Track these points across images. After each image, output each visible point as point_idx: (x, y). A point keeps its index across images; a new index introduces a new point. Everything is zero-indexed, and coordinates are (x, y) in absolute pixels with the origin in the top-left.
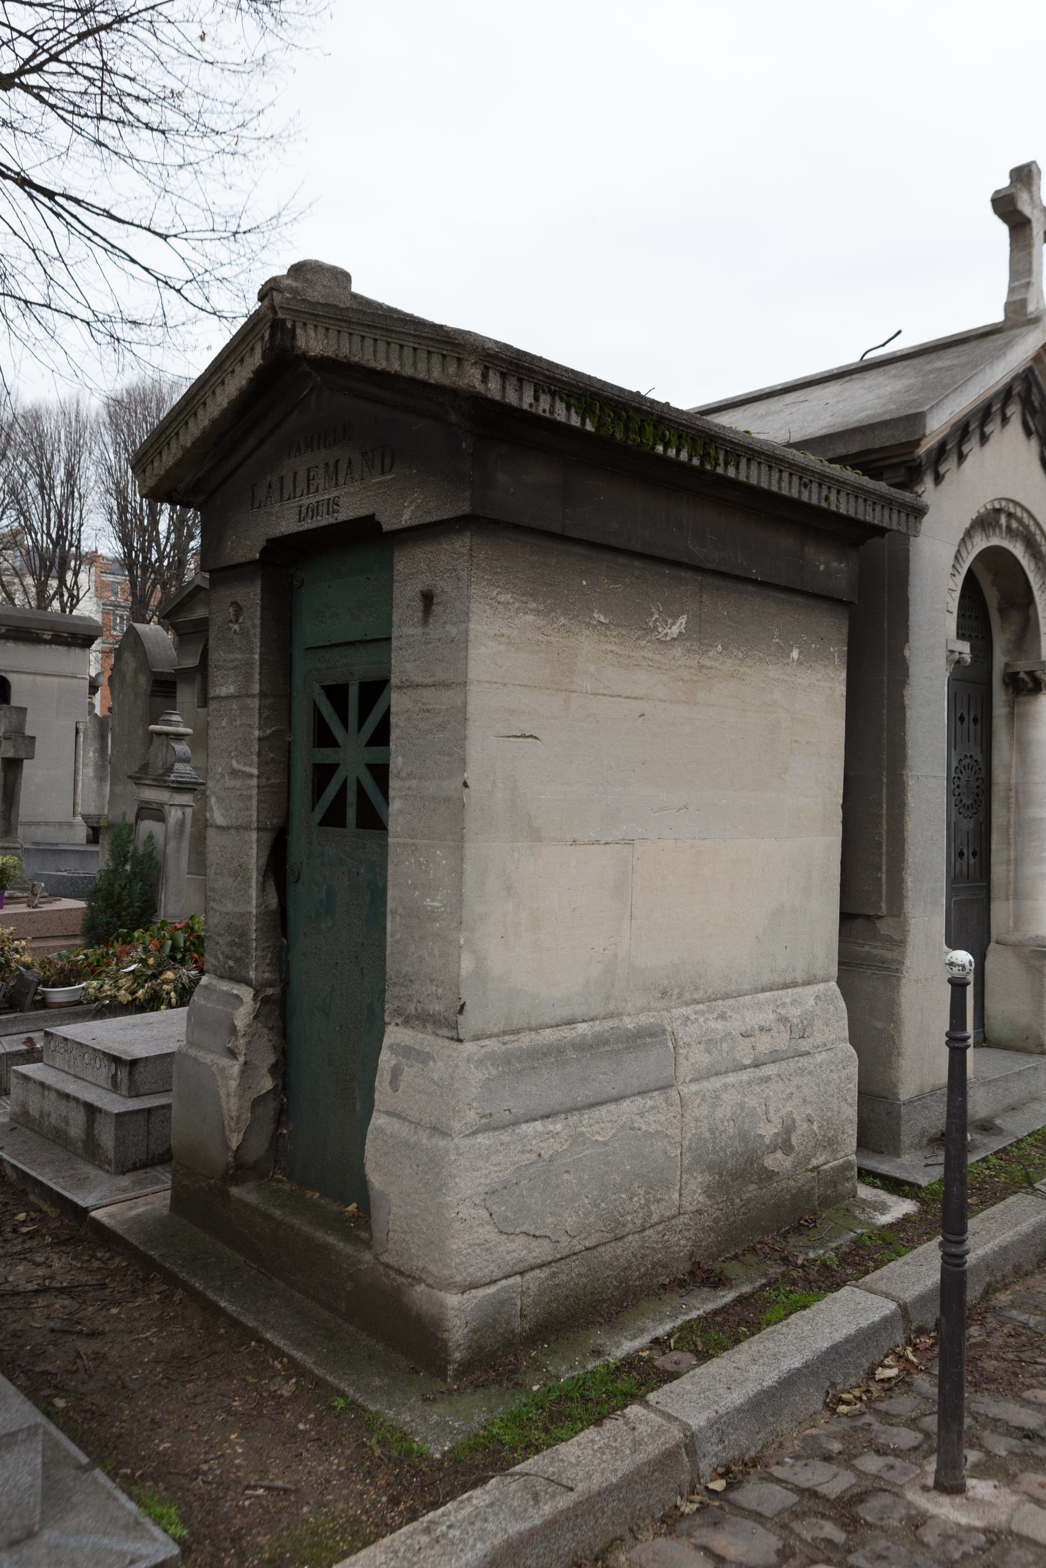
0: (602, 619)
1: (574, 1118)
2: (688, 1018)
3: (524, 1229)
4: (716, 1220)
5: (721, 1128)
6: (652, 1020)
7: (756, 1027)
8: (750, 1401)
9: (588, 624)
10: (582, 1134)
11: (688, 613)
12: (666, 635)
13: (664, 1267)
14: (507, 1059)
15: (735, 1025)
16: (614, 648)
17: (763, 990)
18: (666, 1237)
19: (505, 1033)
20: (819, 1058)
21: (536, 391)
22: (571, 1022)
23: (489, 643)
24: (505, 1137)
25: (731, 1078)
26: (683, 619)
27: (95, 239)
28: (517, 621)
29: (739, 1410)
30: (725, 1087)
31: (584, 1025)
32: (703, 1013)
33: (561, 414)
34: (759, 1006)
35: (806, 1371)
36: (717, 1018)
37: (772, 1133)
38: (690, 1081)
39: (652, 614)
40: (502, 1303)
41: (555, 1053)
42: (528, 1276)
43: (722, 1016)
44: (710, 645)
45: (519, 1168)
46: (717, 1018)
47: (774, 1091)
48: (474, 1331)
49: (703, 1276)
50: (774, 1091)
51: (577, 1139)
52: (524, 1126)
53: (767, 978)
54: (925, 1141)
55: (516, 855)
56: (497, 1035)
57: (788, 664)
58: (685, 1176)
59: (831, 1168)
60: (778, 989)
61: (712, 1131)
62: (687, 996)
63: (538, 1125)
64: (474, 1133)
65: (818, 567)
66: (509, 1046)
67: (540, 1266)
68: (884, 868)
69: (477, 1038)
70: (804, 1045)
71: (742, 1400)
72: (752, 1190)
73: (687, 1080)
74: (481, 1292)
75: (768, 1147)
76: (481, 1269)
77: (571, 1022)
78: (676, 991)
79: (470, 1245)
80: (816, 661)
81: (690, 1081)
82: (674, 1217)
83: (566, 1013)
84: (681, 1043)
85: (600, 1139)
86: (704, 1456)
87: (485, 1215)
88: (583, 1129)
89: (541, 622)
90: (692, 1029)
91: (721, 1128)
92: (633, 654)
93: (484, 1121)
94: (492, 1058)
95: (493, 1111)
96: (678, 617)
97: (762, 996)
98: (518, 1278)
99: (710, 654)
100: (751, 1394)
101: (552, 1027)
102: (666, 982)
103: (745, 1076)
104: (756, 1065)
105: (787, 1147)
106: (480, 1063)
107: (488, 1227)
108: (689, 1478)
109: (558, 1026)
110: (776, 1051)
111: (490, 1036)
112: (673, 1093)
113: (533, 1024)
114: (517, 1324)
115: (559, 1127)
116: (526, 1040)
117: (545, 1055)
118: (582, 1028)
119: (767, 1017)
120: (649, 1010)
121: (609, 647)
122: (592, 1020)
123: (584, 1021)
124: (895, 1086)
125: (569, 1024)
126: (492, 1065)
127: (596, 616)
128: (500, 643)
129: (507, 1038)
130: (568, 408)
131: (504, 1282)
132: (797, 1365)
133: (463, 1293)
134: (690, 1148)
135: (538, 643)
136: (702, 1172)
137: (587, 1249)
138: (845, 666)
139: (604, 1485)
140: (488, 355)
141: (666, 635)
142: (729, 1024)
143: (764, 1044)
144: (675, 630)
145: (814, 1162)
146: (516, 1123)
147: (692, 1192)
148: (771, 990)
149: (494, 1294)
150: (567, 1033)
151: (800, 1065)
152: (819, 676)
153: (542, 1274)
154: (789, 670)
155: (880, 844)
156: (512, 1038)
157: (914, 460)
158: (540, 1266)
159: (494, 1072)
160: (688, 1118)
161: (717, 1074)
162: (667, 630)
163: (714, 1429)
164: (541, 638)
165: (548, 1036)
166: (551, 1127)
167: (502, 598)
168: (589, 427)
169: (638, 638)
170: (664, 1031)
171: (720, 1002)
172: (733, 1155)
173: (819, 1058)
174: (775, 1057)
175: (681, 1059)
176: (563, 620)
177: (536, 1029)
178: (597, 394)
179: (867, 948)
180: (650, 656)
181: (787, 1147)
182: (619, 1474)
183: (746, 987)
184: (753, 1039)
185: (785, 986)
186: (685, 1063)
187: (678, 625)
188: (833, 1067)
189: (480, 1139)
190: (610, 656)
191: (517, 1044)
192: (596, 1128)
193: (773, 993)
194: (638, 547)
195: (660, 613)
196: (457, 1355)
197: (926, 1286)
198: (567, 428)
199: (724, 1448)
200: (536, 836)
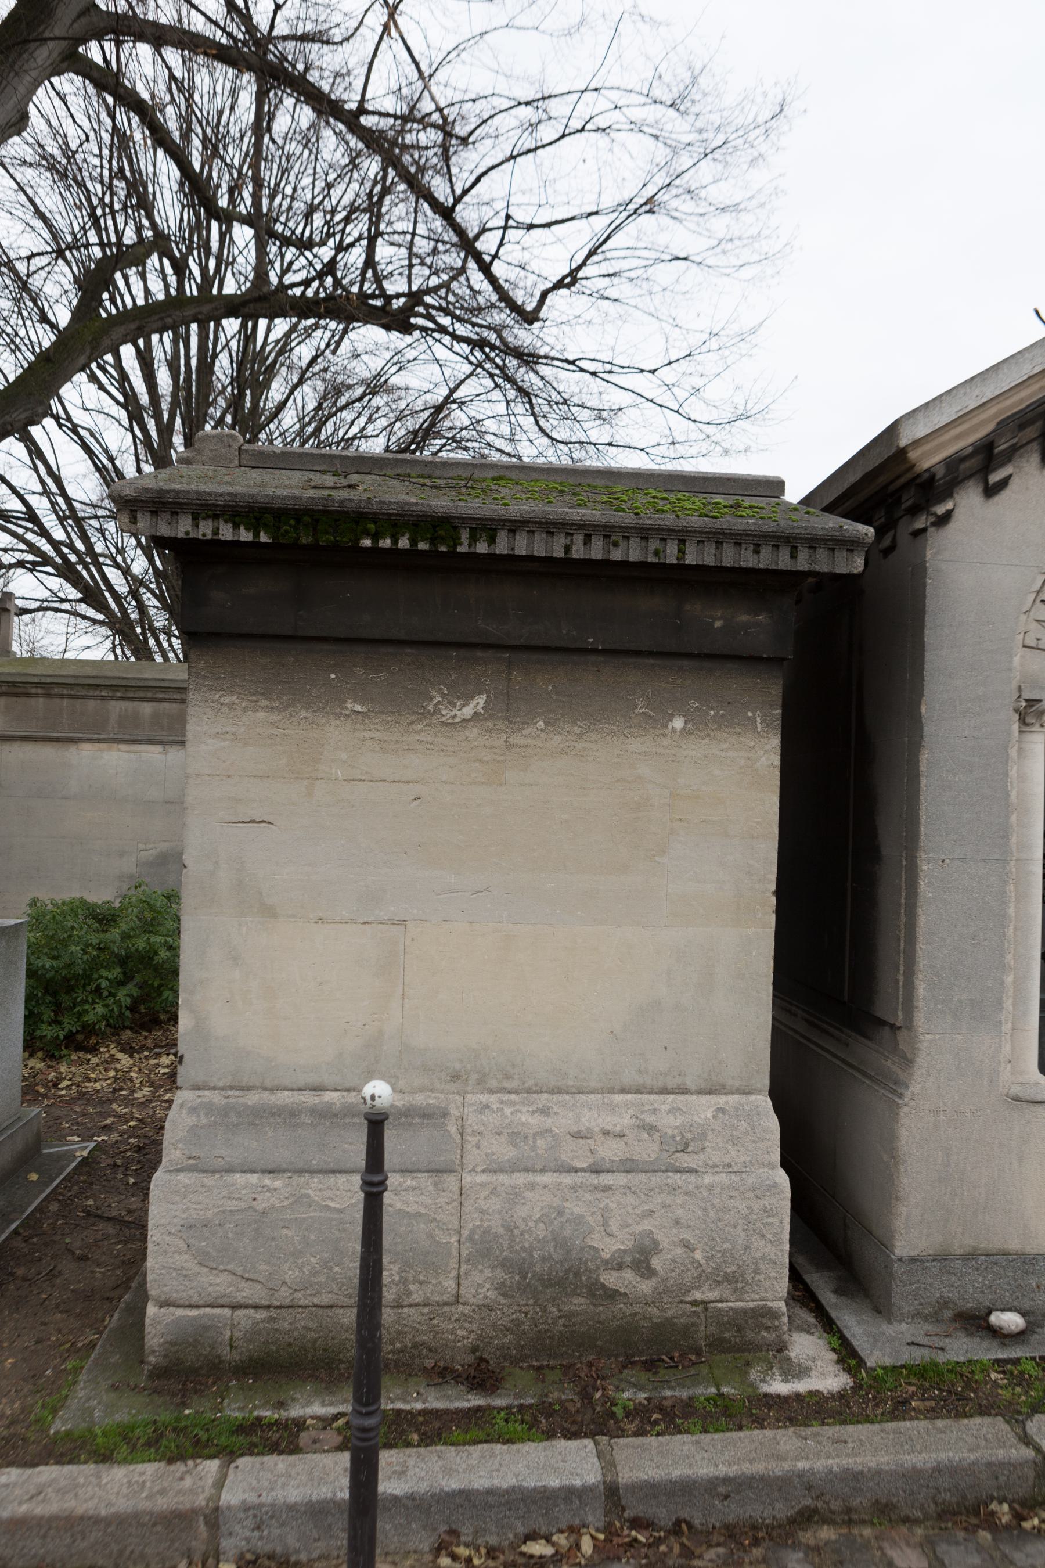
0: (358, 708)
1: (296, 1180)
2: (487, 1107)
3: (229, 1267)
4: (518, 1323)
5: (522, 1227)
6: (431, 1102)
7: (597, 1129)
8: (310, 1504)
9: (338, 716)
10: (308, 1196)
11: (488, 693)
12: (455, 716)
13: (430, 1350)
14: (225, 1111)
15: (563, 1121)
16: (376, 735)
17: (623, 1091)
18: (435, 1322)
19: (231, 1088)
20: (708, 1179)
21: (194, 519)
22: (318, 1089)
23: (210, 741)
24: (209, 1180)
25: (547, 1178)
26: (481, 700)
27: (556, 363)
28: (244, 719)
29: (291, 1508)
30: (532, 1186)
31: (336, 1094)
32: (513, 1104)
33: (227, 533)
34: (612, 1108)
35: (410, 1503)
36: (533, 1112)
37: (615, 1248)
38: (483, 1171)
39: (431, 699)
40: (206, 1328)
41: (290, 1115)
42: (240, 1313)
43: (545, 1111)
44: (524, 723)
45: (224, 1212)
46: (533, 1112)
47: (619, 1203)
48: (172, 1344)
49: (481, 1376)
50: (619, 1203)
51: (300, 1200)
52: (238, 1175)
53: (629, 1077)
54: (948, 1314)
55: (244, 930)
56: (222, 1089)
57: (664, 735)
58: (464, 1267)
59: (732, 1309)
60: (651, 1093)
61: (509, 1229)
62: (493, 1083)
63: (254, 1178)
64: (178, 1170)
65: (712, 624)
66: (231, 1100)
67: (256, 1307)
68: (902, 968)
69: (197, 1088)
70: (685, 1160)
71: (298, 1499)
72: (578, 1303)
73: (479, 1169)
74: (180, 1312)
75: (607, 1262)
76: (177, 1291)
77: (318, 1089)
78: (474, 1077)
79: (164, 1267)
80: (719, 728)
81: (483, 1171)
82: (445, 1304)
83: (313, 1079)
84: (469, 1130)
85: (332, 1204)
86: (231, 1534)
87: (183, 1246)
88: (310, 1192)
89: (274, 717)
90: (489, 1118)
91: (522, 1227)
92: (401, 739)
93: (191, 1162)
94: (209, 1108)
95: (202, 1155)
96: (472, 698)
97: (618, 1098)
98: (227, 1312)
99: (525, 732)
100: (314, 1498)
101: (292, 1090)
102: (458, 1066)
103: (568, 1179)
104: (597, 1171)
105: (644, 1269)
106: (193, 1110)
107: (186, 1257)
108: (203, 1548)
109: (300, 1090)
110: (632, 1160)
111: (214, 1088)
112: (451, 1181)
113: (268, 1083)
114: (225, 1352)
115: (278, 1184)
116: (253, 1098)
117: (273, 1114)
118: (330, 1096)
119: (624, 1121)
120: (432, 1091)
121: (368, 734)
122: (348, 1090)
123: (336, 1090)
124: (892, 1237)
125: (315, 1090)
126: (206, 1114)
127: (349, 706)
128: (224, 740)
129: (230, 1093)
130: (236, 526)
131: (208, 1310)
132: (398, 1492)
133: (161, 1307)
134: (470, 1239)
135: (270, 737)
136: (493, 1268)
137: (316, 1306)
138: (779, 731)
139: (91, 1512)
140: (127, 501)
141: (455, 716)
142: (550, 1120)
143: (611, 1151)
144: (468, 711)
145: (698, 1296)
146: (230, 1170)
147: (481, 1285)
148: (638, 1091)
149: (194, 1318)
150: (310, 1099)
151: (670, 1181)
152: (725, 746)
153: (260, 1315)
154: (666, 742)
155: (899, 939)
156: (237, 1093)
157: (919, 476)
158: (256, 1307)
159: (205, 1121)
160: (468, 1207)
161: (527, 1170)
162: (455, 712)
163: (251, 1512)
164: (275, 731)
165: (285, 1098)
166: (267, 1182)
167: (226, 700)
168: (264, 538)
169: (412, 723)
170: (445, 1114)
171: (545, 1096)
172: (543, 1259)
173: (708, 1179)
174: (629, 1166)
175: (468, 1146)
176: (303, 714)
177: (272, 1090)
178: (266, 508)
179: (889, 1063)
180: (429, 739)
181: (644, 1269)
182: (113, 1510)
183: (593, 1084)
184: (590, 1142)
185: (665, 1091)
186: (475, 1151)
187: (471, 706)
188: (733, 1193)
189: (181, 1177)
190: (369, 743)
191: (241, 1100)
192: (329, 1193)
193: (639, 1096)
194: (402, 636)
195: (443, 695)
196: (152, 1359)
197: (670, 1473)
198: (236, 544)
199: (261, 1538)
200: (269, 912)
